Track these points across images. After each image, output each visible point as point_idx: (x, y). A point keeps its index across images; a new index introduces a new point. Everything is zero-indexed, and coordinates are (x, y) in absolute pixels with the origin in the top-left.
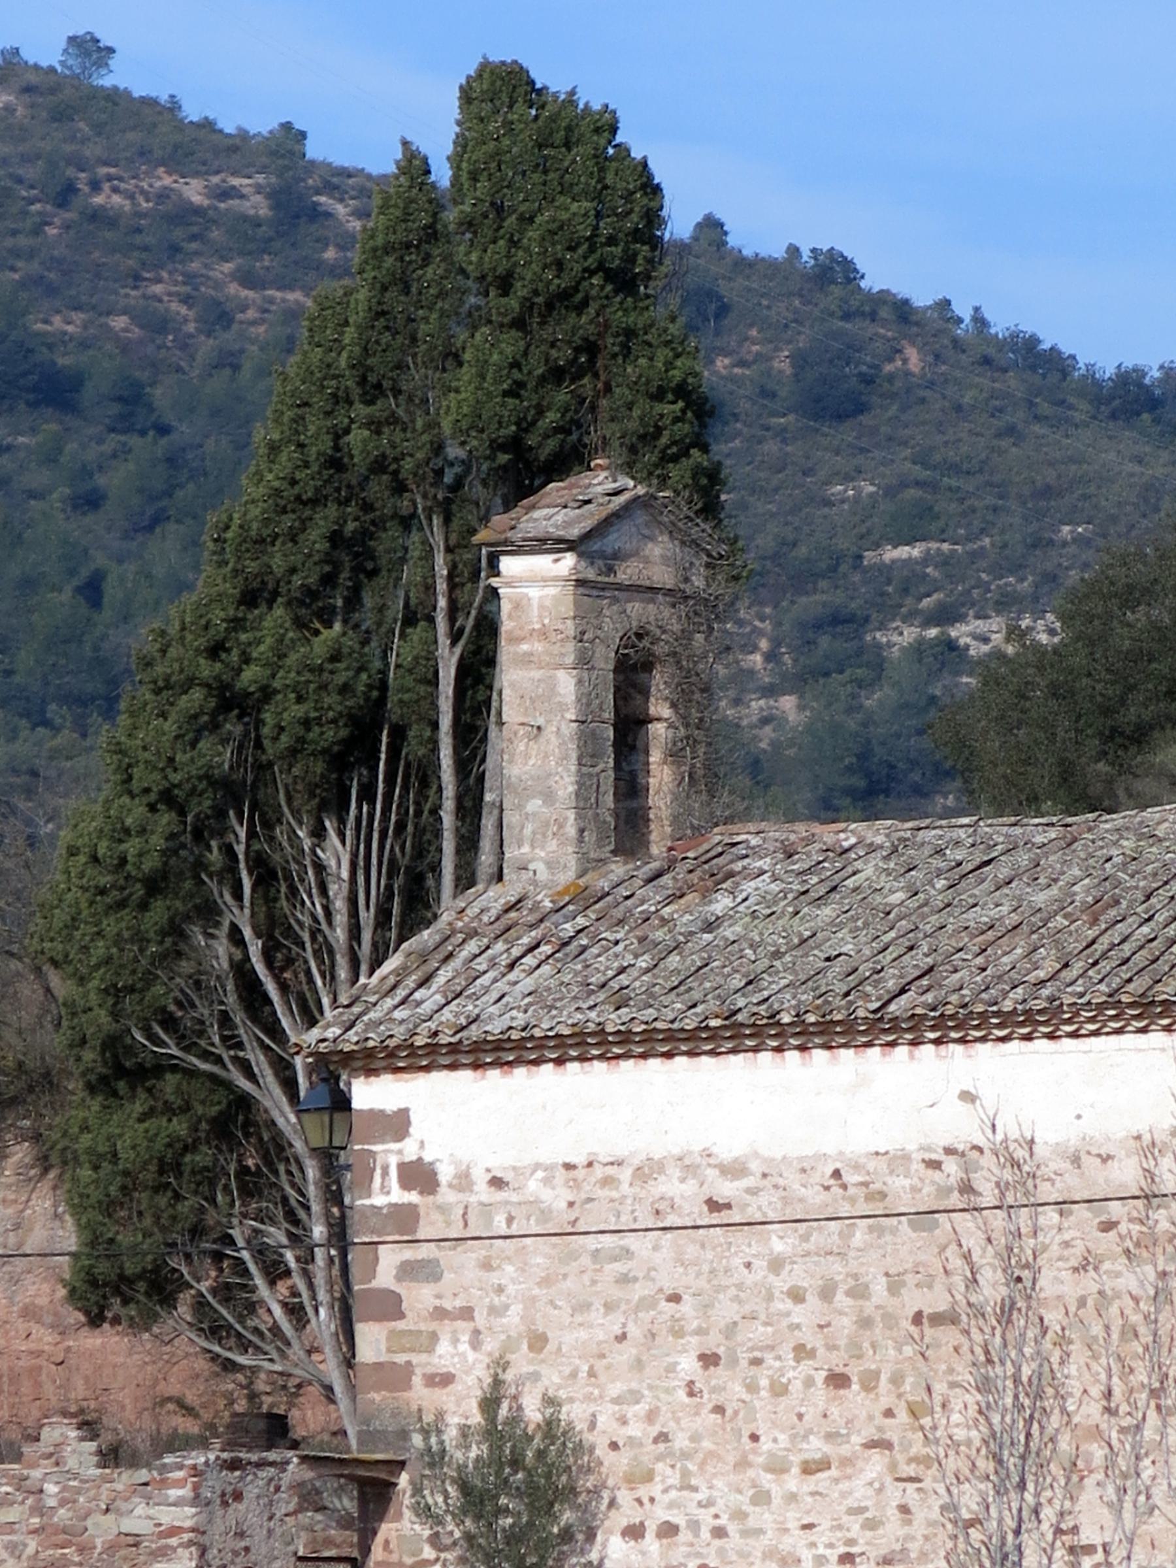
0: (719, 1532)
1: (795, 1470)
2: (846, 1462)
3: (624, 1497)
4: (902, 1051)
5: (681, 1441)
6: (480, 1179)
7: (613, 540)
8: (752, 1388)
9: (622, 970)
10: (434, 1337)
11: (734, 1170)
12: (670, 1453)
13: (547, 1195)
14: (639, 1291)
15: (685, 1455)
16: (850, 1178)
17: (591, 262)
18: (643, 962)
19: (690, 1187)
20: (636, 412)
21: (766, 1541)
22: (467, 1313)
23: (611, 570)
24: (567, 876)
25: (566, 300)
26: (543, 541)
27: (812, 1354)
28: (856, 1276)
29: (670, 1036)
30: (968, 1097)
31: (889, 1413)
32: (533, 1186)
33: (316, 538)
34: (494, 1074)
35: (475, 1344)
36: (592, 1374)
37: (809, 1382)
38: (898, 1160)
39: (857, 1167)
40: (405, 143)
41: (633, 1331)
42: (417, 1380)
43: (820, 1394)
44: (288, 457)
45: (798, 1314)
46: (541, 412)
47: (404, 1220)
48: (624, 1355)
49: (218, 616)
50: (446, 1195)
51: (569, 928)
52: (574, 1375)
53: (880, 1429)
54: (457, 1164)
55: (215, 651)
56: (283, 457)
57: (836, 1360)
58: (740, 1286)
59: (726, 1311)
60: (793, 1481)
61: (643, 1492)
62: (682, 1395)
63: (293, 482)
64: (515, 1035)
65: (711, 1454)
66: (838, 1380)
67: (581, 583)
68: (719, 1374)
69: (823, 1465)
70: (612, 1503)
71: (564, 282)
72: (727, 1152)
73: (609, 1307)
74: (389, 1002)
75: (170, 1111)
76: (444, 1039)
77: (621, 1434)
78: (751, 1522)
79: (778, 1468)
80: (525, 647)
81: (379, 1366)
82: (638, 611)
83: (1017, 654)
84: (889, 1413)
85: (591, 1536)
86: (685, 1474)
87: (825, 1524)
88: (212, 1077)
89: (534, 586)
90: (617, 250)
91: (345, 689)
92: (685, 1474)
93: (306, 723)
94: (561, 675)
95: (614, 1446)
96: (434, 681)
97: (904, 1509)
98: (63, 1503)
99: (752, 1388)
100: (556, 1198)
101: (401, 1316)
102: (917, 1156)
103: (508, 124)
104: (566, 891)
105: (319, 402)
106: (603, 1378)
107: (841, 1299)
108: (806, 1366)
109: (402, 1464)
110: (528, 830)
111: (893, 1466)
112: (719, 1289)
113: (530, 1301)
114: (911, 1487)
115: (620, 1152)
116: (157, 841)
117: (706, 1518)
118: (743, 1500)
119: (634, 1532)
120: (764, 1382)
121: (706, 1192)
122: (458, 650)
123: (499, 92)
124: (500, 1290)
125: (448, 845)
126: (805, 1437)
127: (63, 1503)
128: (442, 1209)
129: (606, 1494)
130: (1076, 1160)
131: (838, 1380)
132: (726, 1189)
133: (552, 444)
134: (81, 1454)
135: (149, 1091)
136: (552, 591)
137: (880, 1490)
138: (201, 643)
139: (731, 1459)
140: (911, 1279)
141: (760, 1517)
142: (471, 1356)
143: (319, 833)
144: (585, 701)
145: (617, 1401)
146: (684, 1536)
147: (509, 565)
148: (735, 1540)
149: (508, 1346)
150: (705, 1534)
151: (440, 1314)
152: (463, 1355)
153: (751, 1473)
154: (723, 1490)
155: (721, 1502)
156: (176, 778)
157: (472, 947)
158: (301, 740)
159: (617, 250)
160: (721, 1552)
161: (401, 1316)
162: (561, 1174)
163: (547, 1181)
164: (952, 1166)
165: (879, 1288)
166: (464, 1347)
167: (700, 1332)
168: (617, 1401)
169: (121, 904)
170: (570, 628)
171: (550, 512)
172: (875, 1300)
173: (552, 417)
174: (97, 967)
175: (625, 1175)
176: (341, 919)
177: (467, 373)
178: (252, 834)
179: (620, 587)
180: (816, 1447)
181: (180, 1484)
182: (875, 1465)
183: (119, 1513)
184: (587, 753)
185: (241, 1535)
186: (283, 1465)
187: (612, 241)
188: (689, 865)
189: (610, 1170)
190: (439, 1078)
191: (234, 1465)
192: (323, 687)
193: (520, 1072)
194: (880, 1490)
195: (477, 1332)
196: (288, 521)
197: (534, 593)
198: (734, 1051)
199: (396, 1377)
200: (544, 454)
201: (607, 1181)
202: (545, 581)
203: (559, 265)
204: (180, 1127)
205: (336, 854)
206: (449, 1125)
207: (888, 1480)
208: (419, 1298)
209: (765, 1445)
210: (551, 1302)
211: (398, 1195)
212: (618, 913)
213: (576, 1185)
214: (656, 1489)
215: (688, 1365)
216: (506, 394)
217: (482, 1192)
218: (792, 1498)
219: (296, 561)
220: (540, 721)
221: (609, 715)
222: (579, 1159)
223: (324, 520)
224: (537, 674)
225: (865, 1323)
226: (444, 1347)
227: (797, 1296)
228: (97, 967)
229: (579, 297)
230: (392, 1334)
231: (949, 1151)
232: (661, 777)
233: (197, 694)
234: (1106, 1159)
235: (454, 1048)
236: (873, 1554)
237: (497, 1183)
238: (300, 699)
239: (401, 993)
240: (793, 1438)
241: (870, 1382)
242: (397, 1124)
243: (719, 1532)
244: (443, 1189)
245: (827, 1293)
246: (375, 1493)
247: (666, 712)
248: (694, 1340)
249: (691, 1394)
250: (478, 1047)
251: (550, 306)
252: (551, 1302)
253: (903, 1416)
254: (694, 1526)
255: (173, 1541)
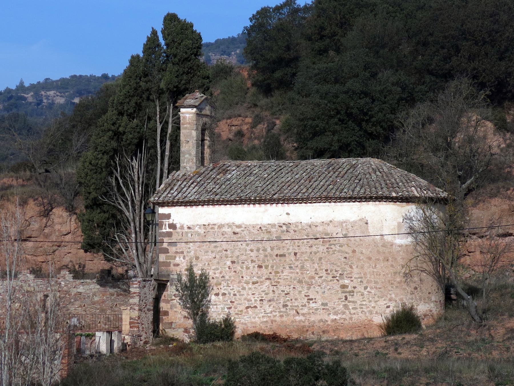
0: (235, 295)
1: (251, 283)
2: (261, 282)
3: (215, 288)
4: (274, 205)
5: (227, 277)
6: (185, 227)
7: (201, 106)
8: (242, 268)
9: (213, 188)
10: (175, 257)
11: (239, 226)
12: (225, 280)
13: (200, 230)
14: (219, 249)
15: (228, 280)
16: (263, 229)
17: (192, 52)
18: (217, 187)
19: (230, 230)
20: (200, 81)
21: (244, 296)
22: (182, 253)
23: (201, 112)
24: (194, 170)
25: (187, 59)
26: (190, 106)
27: (255, 262)
28: (264, 247)
29: (228, 201)
30: (288, 214)
31: (271, 273)
32: (197, 229)
33: (133, 103)
34: (189, 207)
35: (184, 258)
36: (208, 264)
37: (254, 267)
38: (273, 226)
39: (265, 227)
40: (153, 28)
41: (217, 256)
42: (172, 265)
43: (256, 269)
44: (127, 87)
45: (252, 254)
46: (181, 80)
47: (169, 234)
48: (216, 261)
49: (114, 118)
50: (178, 230)
51: (198, 180)
52: (205, 264)
53: (269, 276)
54: (181, 224)
55: (113, 124)
56: (127, 87)
57: (260, 263)
58: (240, 249)
59: (237, 253)
60: (250, 286)
61: (219, 287)
62: (227, 269)
63: (129, 92)
64: (195, 200)
65: (233, 280)
66: (260, 267)
67: (197, 114)
68: (235, 265)
69: (257, 282)
70: (212, 289)
71: (186, 56)
72: (238, 223)
73: (212, 252)
74: (166, 193)
75: (104, 212)
76: (180, 201)
77: (214, 276)
78: (242, 293)
79: (247, 283)
80: (185, 126)
81: (163, 262)
82: (205, 119)
83: (80, 101)
84: (271, 273)
85: (208, 295)
86: (228, 284)
87: (257, 294)
88: (114, 206)
89: (187, 114)
90: (196, 50)
91: (139, 132)
92: (228, 284)
93: (132, 138)
94: (193, 131)
95: (213, 278)
96: (156, 131)
97: (273, 291)
98: (65, 286)
99: (242, 268)
100: (202, 231)
101: (169, 253)
102: (277, 225)
103: (174, 25)
104: (194, 172)
105: (134, 77)
106: (211, 265)
107: (261, 251)
108: (253, 264)
109: (168, 281)
110: (186, 160)
111: (271, 283)
112: (235, 249)
113: (196, 251)
114: (275, 287)
115: (215, 222)
116: (105, 161)
117: (232, 292)
118: (240, 289)
119: (217, 295)
120: (245, 267)
121: (233, 230)
122: (161, 125)
123: (171, 19)
124: (189, 248)
125: (159, 163)
126: (253, 277)
127: (65, 286)
128: (177, 233)
129: (211, 288)
130: (310, 226)
131: (260, 267)
132: (237, 230)
133: (183, 87)
134: (69, 277)
135: (100, 208)
136: (191, 115)
137: (268, 288)
138: (111, 123)
139: (238, 281)
140: (275, 248)
141: (243, 292)
142: (183, 261)
143: (132, 160)
144: (197, 136)
145: (213, 270)
146: (227, 295)
147: (182, 110)
148: (238, 296)
149: (191, 259)
150: (232, 295)
151: (177, 252)
152: (181, 261)
153: (242, 284)
154: (236, 287)
155: (235, 289)
156: (107, 148)
157: (180, 183)
158: (131, 142)
159: (196, 50)
160: (235, 299)
161: (169, 253)
162: (202, 227)
163: (200, 228)
164: (284, 228)
165: (269, 250)
166: (182, 259)
167: (231, 257)
168: (213, 270)
169: (96, 173)
170: (195, 122)
171: (190, 101)
172: (268, 252)
173: (183, 82)
174: (92, 184)
175: (216, 227)
176: (136, 176)
177: (168, 73)
178: (119, 159)
179: (203, 115)
180: (255, 279)
181: (136, 284)
182: (268, 283)
183: (77, 288)
184: (197, 147)
185: (145, 294)
186: (151, 281)
187: (195, 48)
188: (218, 168)
189: (213, 226)
190: (177, 208)
191: (144, 281)
192: (135, 132)
193: (194, 207)
194: (268, 288)
195: (184, 256)
196: (128, 100)
197: (187, 115)
198: (239, 204)
199: (168, 264)
200: (182, 88)
201: (212, 228)
202: (192, 113)
203: (186, 53)
204: (107, 215)
205: (135, 163)
206: (180, 216)
207: (270, 286)
208: (172, 249)
209: (245, 278)
210: (200, 251)
211: (168, 230)
212: (208, 176)
213: (206, 229)
214: (222, 287)
215: (229, 263)
216: (176, 77)
217: (186, 230)
218: (250, 289)
219: (129, 107)
220: (189, 140)
221: (200, 139)
222: (206, 224)
223: (134, 100)
224: (188, 131)
225: (266, 256)
226: (177, 259)
227: (252, 251)
228: (92, 184)
229: (189, 59)
230: (166, 256)
231: (284, 224)
232: (207, 151)
233: (111, 132)
234: (316, 226)
235: (182, 202)
236: (267, 299)
237: (189, 228)
238: (131, 134)
239: (168, 192)
240: (250, 277)
241: (267, 267)
242: (168, 216)
243: (235, 295)
244: (178, 229)
245: (258, 250)
246: (162, 286)
247: (208, 139)
248: (230, 258)
249: (229, 269)
250: (187, 202)
251: (184, 60)
252: (200, 251)
253: (273, 274)
254: (230, 294)
255: (135, 295)
